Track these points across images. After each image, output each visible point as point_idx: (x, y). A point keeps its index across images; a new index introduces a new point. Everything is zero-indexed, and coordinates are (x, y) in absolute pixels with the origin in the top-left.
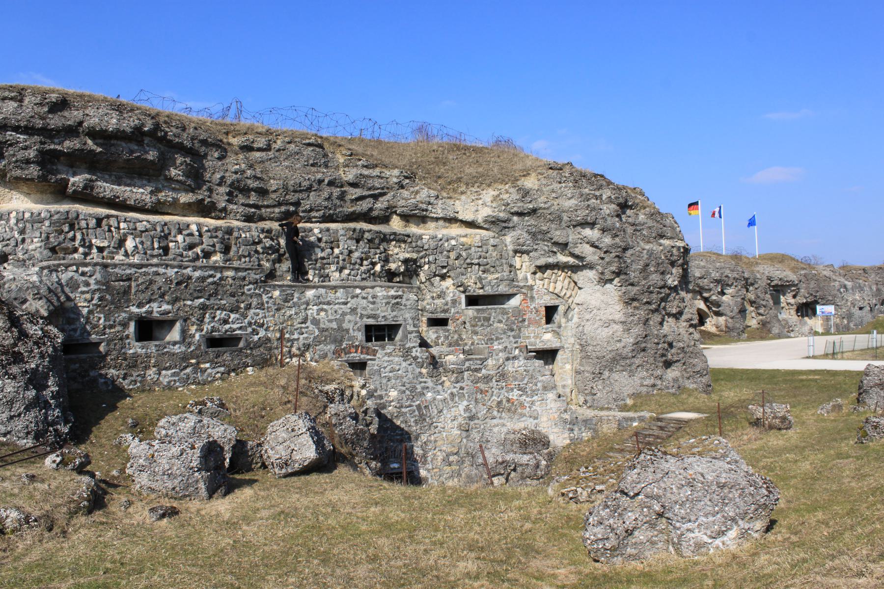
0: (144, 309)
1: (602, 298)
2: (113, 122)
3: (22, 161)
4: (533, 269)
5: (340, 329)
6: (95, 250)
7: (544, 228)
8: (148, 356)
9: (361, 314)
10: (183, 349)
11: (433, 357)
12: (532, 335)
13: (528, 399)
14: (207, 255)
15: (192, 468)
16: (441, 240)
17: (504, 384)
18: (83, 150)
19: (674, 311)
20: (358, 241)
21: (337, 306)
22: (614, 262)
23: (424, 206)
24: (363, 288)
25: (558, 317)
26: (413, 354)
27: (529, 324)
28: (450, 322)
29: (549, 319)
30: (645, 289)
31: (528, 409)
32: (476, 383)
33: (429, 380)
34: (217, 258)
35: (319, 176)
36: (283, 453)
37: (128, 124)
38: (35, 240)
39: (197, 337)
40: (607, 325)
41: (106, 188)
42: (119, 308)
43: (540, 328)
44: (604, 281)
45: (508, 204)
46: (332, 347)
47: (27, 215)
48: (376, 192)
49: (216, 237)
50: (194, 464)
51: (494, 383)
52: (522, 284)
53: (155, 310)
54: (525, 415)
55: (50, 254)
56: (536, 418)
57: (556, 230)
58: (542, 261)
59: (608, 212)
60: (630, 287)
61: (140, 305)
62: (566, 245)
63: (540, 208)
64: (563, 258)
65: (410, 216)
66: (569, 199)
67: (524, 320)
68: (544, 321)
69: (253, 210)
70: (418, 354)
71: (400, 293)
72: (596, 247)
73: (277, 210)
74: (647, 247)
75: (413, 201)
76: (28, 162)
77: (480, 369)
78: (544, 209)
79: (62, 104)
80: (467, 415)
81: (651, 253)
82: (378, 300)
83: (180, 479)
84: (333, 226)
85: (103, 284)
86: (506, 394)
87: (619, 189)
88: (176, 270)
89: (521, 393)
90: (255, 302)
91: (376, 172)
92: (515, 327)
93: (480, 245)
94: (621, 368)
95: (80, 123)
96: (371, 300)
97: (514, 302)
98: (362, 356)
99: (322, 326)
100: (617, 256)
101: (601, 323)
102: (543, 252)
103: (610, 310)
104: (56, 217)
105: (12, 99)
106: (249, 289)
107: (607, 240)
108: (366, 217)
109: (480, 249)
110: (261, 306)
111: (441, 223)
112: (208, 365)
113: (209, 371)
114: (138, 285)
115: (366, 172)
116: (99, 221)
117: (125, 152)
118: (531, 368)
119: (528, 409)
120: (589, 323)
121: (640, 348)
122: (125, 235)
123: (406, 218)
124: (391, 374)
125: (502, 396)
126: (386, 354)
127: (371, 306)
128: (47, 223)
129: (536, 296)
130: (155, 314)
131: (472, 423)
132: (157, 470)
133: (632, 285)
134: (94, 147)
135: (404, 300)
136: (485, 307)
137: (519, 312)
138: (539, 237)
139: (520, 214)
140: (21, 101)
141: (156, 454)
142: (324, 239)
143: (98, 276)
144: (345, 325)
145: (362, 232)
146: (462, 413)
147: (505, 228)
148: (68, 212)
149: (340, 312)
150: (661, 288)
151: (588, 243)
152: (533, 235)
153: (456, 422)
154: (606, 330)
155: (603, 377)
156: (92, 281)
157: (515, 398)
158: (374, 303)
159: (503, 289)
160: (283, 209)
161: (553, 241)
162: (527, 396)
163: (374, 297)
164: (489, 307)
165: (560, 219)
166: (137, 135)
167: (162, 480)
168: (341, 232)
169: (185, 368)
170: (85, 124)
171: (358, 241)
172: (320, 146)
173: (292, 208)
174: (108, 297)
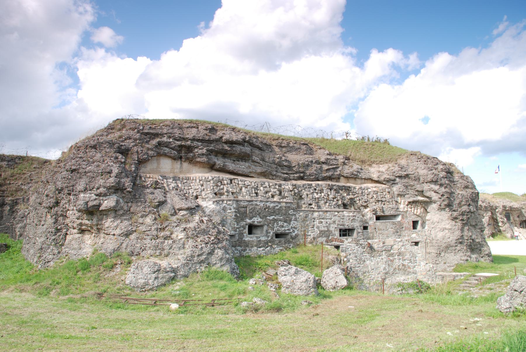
0: (252, 221)
1: (440, 217)
2: (235, 137)
3: (200, 155)
4: (406, 203)
5: (328, 230)
6: (231, 194)
7: (412, 184)
8: (253, 241)
9: (338, 224)
10: (266, 238)
11: (369, 244)
12: (407, 235)
13: (412, 265)
14: (273, 196)
15: (310, 287)
16: (364, 189)
17: (401, 257)
18: (222, 149)
19: (474, 224)
20: (331, 190)
21: (327, 220)
22: (446, 200)
23: (356, 173)
24: (338, 212)
25: (419, 227)
26: (361, 243)
27: (405, 229)
28: (369, 228)
29: (414, 227)
30: (461, 213)
31: (412, 269)
32: (389, 256)
33: (367, 255)
34: (276, 199)
35: (311, 159)
36: (333, 283)
37: (239, 137)
38: (208, 189)
39: (272, 233)
40: (442, 230)
41: (231, 165)
42: (242, 220)
43: (410, 232)
44: (440, 209)
45: (395, 172)
46: (325, 239)
47: (203, 178)
48: (334, 166)
49: (276, 188)
50: (311, 285)
51: (396, 257)
52: (401, 210)
53: (256, 221)
54: (410, 272)
55: (214, 195)
56: (416, 274)
57: (417, 184)
58: (411, 200)
59: (442, 176)
60: (453, 212)
61: (251, 219)
62: (423, 191)
63: (410, 174)
64: (420, 198)
65: (350, 178)
66: (423, 170)
67: (403, 228)
68: (412, 227)
69: (286, 175)
70: (363, 243)
71: (355, 214)
72: (437, 193)
73: (296, 175)
74: (460, 193)
75: (351, 171)
76: (203, 154)
77: (390, 250)
78: (411, 174)
79: (213, 130)
80: (385, 271)
81: (463, 196)
82: (345, 218)
83: (305, 291)
84: (320, 183)
85: (236, 209)
86: (402, 262)
87: (444, 164)
88: (264, 203)
89: (409, 262)
90: (293, 218)
91: (333, 157)
92: (398, 231)
93: (382, 191)
94: (450, 251)
95: (221, 137)
96: (342, 217)
97: (399, 219)
98: (338, 243)
99: (320, 229)
100: (447, 197)
101: (439, 229)
102: (411, 195)
103: (443, 223)
104: (215, 179)
105: (194, 127)
106: (291, 212)
107: (443, 190)
108: (330, 178)
109: (382, 194)
110: (296, 220)
111: (363, 181)
112: (276, 246)
113: (276, 249)
114: (249, 210)
115: (329, 157)
116: (231, 180)
117: (238, 149)
118: (413, 250)
119: (412, 269)
120: (433, 229)
121: (460, 241)
122: (242, 187)
123: (347, 178)
124: (351, 252)
125: (400, 263)
126: (348, 242)
127: (342, 220)
128: (212, 182)
129: (408, 216)
130: (256, 223)
131: (387, 275)
132: (295, 287)
133: (454, 211)
134: (227, 148)
135: (356, 217)
136: (385, 221)
137: (400, 224)
138: (409, 188)
139: (400, 177)
140: (198, 128)
141: (295, 281)
142: (317, 189)
143: (235, 205)
144: (331, 229)
145: (333, 185)
146: (382, 270)
147: (393, 183)
148: (219, 177)
149: (328, 223)
150: (468, 212)
151: (433, 191)
152: (406, 187)
153: (379, 275)
154: (442, 233)
155: (441, 255)
156: (232, 208)
157: (406, 264)
158: (343, 219)
159: (392, 213)
160: (298, 175)
161: (416, 190)
162: (412, 263)
163: (344, 216)
164: (387, 221)
165: (419, 179)
166: (243, 142)
167: (298, 291)
168: (324, 186)
169: (267, 247)
170: (223, 138)
171: (331, 190)
172: (307, 144)
173: (302, 175)
174: (238, 215)
